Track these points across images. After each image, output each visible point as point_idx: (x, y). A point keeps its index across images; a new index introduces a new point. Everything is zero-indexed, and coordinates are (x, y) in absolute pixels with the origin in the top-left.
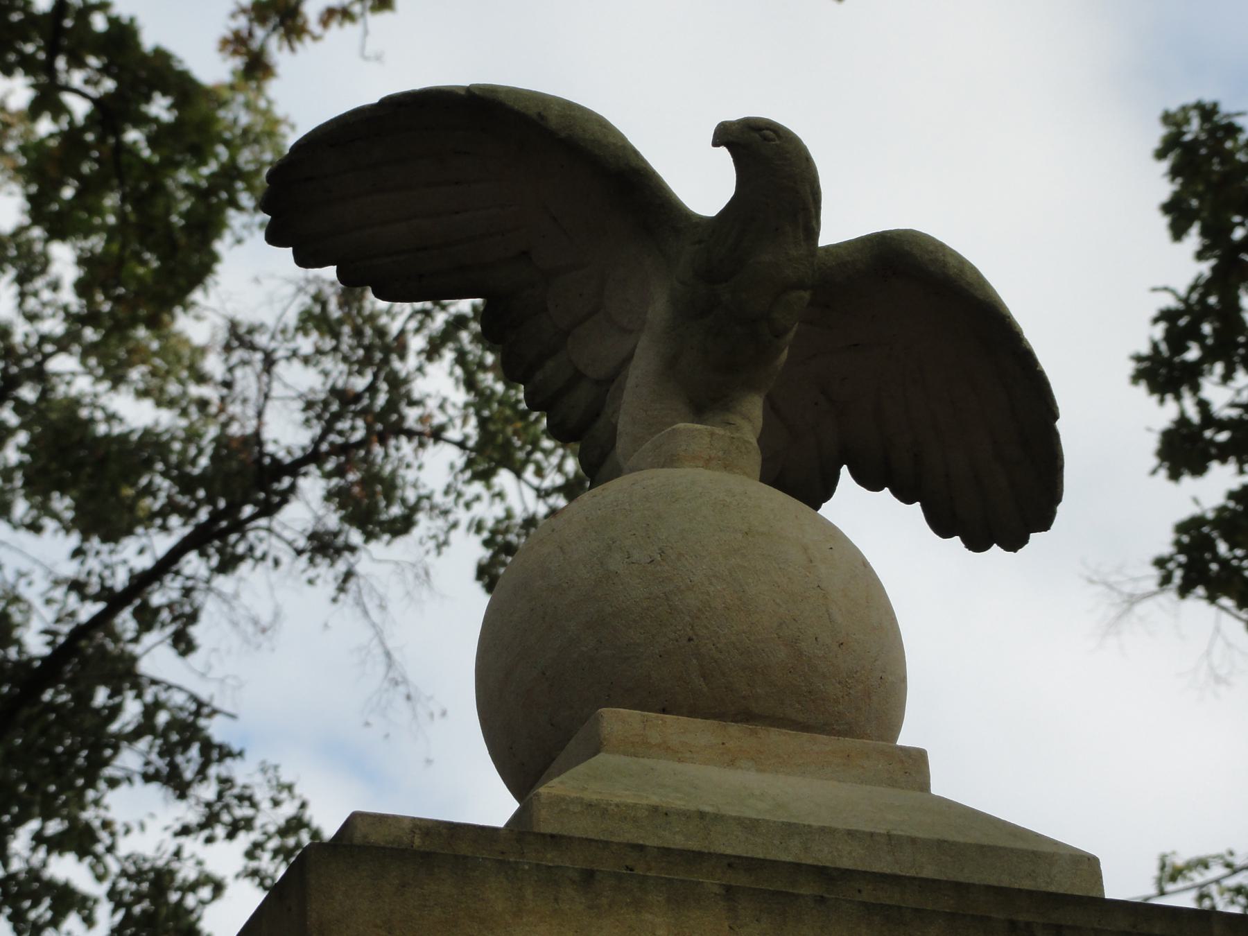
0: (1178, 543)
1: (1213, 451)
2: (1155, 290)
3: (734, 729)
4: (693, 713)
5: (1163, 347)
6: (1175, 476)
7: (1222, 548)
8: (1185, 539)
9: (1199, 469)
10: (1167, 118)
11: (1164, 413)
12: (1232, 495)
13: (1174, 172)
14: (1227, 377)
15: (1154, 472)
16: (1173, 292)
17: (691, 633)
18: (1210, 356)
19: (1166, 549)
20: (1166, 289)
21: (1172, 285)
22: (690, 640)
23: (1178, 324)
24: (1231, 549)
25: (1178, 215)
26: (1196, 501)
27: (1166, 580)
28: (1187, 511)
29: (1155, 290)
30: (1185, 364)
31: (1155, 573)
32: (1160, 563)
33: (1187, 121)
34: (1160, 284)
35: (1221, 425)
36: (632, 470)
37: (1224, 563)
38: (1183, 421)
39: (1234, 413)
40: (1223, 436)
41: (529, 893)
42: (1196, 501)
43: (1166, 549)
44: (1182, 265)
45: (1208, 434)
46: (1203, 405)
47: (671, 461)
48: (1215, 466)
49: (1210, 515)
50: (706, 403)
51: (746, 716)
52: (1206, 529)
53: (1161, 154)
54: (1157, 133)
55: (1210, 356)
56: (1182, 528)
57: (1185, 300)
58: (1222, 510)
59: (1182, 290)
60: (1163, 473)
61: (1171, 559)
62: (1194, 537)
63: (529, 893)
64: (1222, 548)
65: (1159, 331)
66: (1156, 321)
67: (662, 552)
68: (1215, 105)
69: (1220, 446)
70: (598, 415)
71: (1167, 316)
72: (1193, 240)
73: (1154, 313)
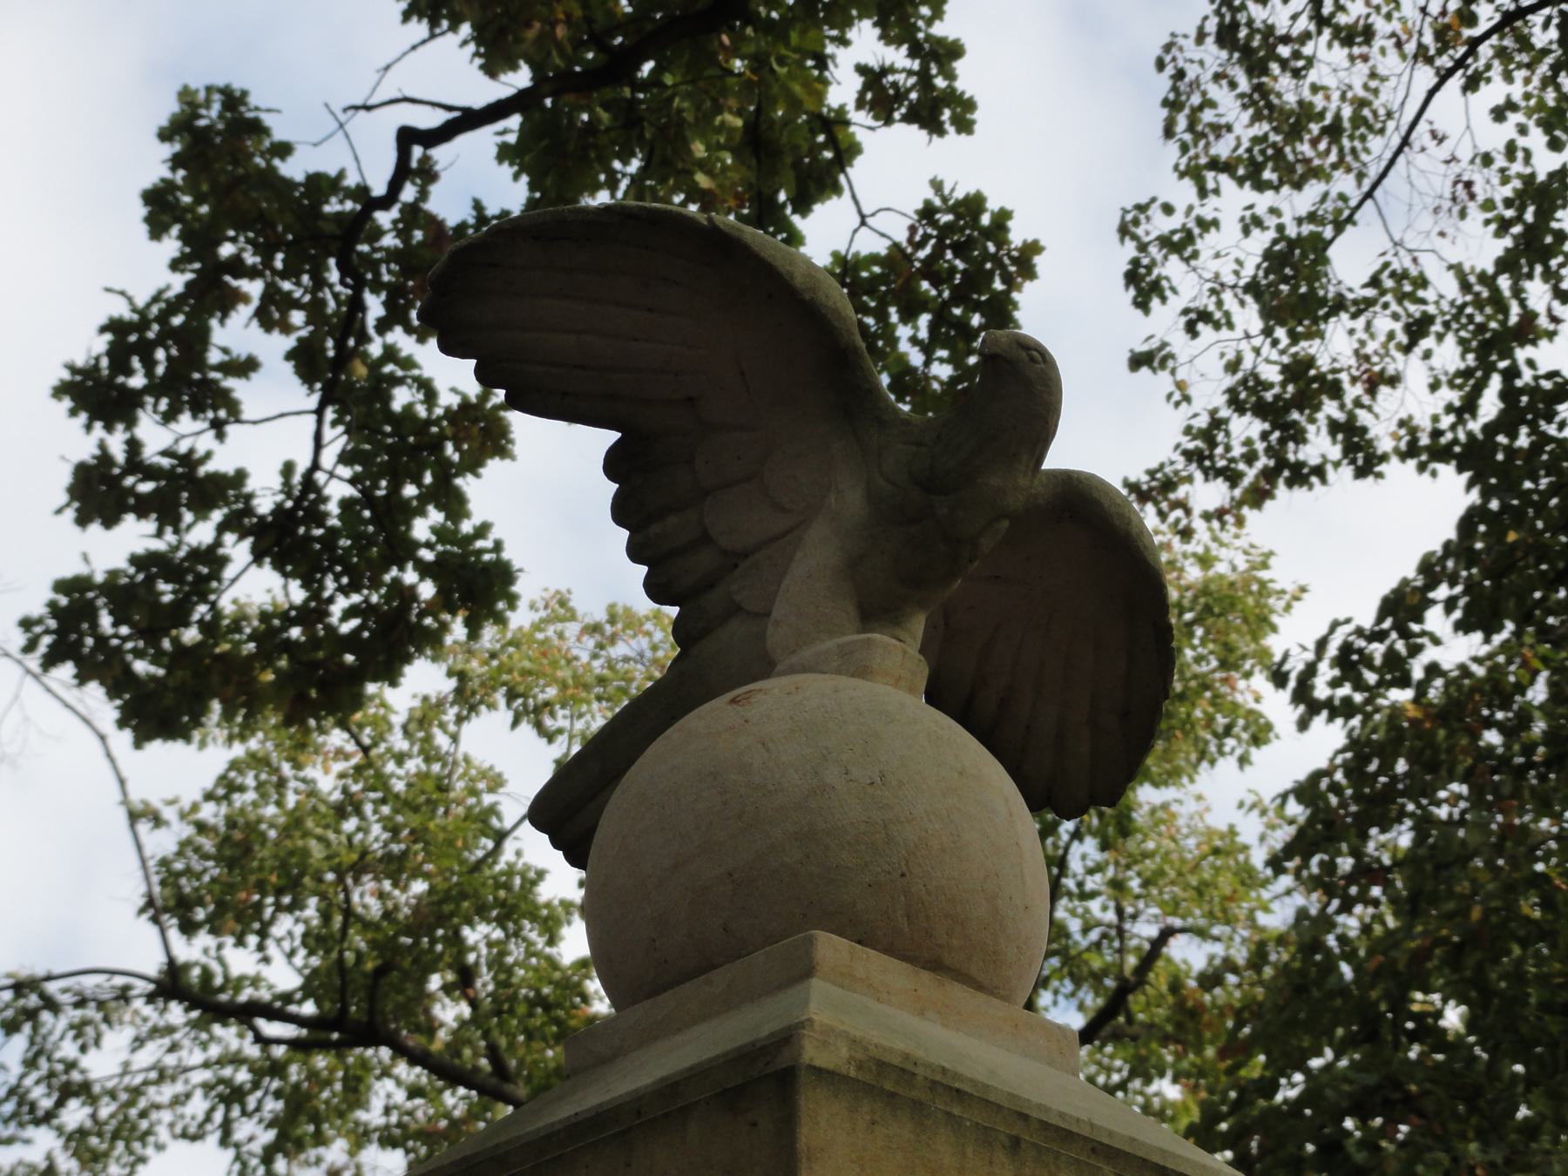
0: (52, 605)
1: (132, 501)
2: (108, 290)
3: (926, 976)
4: (889, 951)
5: (105, 362)
6: (82, 520)
7: (106, 621)
8: (63, 601)
9: (110, 521)
10: (186, 95)
11: (79, 441)
12: (135, 560)
13: (176, 162)
14: (169, 417)
15: (59, 511)
16: (130, 299)
17: (904, 869)
18: (156, 388)
19: (37, 609)
20: (122, 293)
21: (131, 293)
22: (903, 875)
23: (126, 338)
24: (116, 624)
25: (160, 208)
26: (86, 558)
27: (30, 647)
28: (71, 568)
29: (108, 290)
30: (124, 389)
31: (19, 639)
32: (26, 624)
33: (208, 104)
34: (118, 287)
35: (150, 472)
36: (792, 670)
37: (102, 640)
38: (105, 458)
39: (166, 462)
40: (146, 487)
41: (969, 1150)
42: (86, 558)
43: (37, 609)
44: (153, 269)
45: (129, 481)
46: (134, 446)
47: (863, 672)
48: (130, 518)
49: (99, 578)
50: (877, 611)
51: (936, 966)
52: (91, 595)
53: (165, 136)
54: (167, 108)
55: (156, 388)
56: (61, 586)
57: (143, 313)
58: (113, 574)
59: (141, 302)
60: (70, 514)
61: (39, 621)
62: (75, 604)
63: (969, 1150)
64: (106, 621)
65: (102, 343)
66: (103, 329)
67: (882, 776)
68: (245, 93)
69: (140, 498)
70: (712, 586)
71: (115, 327)
72: (171, 246)
73: (103, 320)
